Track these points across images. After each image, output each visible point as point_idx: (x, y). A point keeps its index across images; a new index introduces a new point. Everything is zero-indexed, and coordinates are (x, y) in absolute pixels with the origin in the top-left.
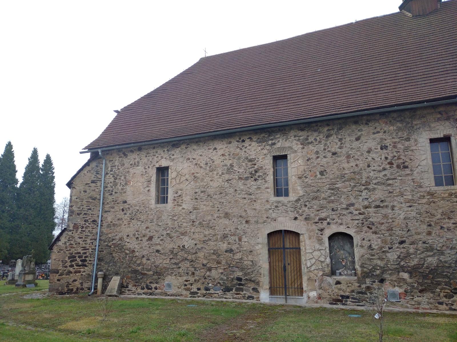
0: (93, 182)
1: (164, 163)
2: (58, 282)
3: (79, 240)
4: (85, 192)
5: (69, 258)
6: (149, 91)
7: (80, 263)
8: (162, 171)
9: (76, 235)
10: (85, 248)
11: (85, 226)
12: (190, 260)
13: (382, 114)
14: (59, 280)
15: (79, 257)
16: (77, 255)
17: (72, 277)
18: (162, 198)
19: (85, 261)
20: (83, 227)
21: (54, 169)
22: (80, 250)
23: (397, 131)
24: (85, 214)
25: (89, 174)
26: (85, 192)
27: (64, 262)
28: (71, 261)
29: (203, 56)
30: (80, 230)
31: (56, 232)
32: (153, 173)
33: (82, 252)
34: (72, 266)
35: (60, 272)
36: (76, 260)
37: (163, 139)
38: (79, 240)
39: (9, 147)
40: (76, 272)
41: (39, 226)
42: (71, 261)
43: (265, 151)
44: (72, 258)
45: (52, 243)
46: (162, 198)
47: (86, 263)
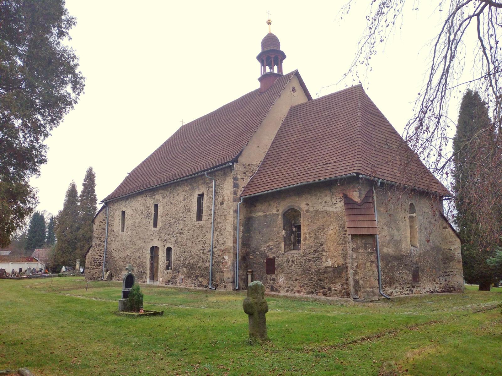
0: (104, 220)
1: (124, 209)
3: (98, 252)
4: (100, 225)
5: (93, 261)
8: (123, 213)
9: (96, 249)
10: (100, 256)
15: (98, 261)
17: (95, 271)
19: (100, 263)
22: (98, 257)
25: (102, 216)
26: (100, 225)
27: (91, 263)
28: (94, 263)
29: (181, 126)
31: (492, 122)
32: (121, 213)
34: (94, 265)
37: (177, 179)
38: (98, 252)
40: (96, 269)
41: (68, 248)
42: (94, 263)
43: (152, 202)
44: (95, 261)
45: (493, 125)
46: (123, 230)
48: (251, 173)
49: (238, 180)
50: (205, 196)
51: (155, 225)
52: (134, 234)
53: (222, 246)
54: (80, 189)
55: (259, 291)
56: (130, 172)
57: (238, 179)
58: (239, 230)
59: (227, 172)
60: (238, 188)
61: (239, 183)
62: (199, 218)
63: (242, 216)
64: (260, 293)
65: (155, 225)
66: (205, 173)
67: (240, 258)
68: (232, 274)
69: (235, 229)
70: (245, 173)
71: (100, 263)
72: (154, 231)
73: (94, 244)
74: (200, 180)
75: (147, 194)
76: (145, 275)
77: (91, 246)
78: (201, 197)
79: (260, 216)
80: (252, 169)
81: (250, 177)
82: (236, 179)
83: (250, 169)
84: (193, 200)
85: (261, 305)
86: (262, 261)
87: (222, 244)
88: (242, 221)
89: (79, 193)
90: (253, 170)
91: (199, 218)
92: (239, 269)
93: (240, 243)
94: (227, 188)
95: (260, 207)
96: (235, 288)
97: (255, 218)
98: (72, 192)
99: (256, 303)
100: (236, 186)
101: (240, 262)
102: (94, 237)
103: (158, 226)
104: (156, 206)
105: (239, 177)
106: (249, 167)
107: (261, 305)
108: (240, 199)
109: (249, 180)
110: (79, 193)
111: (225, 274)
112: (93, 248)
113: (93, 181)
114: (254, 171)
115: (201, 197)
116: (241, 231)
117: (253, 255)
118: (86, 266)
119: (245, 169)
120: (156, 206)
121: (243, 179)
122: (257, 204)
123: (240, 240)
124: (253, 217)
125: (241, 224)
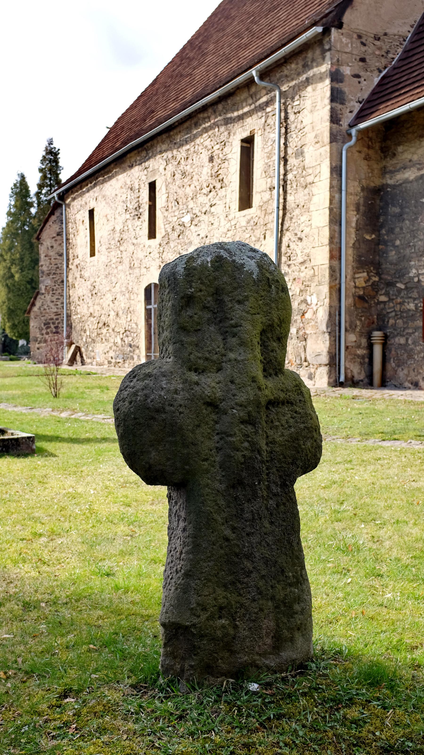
1: (92, 205)
2: (38, 351)
4: (52, 247)
5: (45, 324)
6: (213, 10)
7: (54, 330)
8: (91, 213)
11: (55, 288)
12: (308, 186)
13: (294, 55)
14: (38, 349)
15: (53, 323)
16: (51, 322)
18: (93, 254)
20: (53, 290)
21: (3, 229)
23: (381, 253)
24: (54, 274)
27: (41, 329)
30: (51, 292)
33: (55, 317)
34: (47, 333)
35: (39, 339)
36: (50, 327)
38: (51, 305)
39: (23, 177)
44: (47, 324)
46: (93, 254)
47: (59, 330)
48: (384, 61)
49: (341, 81)
50: (258, 140)
51: (152, 234)
52: (114, 260)
53: (303, 268)
54: (33, 182)
55: (238, 312)
56: (111, 125)
57: (343, 75)
58: (347, 222)
59: (313, 60)
60: (342, 103)
61: (346, 90)
62: (246, 202)
63: (356, 184)
64: (251, 330)
65: (152, 234)
66: (254, 73)
67: (351, 300)
68: (328, 343)
69: (335, 219)
70: (363, 60)
71: (56, 327)
72: (150, 246)
73: (42, 287)
74: (245, 100)
75: (133, 160)
76: (137, 351)
77: (38, 293)
78: (248, 144)
79: (406, 181)
80: (385, 47)
81: (380, 72)
82: (336, 77)
83: (380, 49)
84: (229, 156)
85: (250, 421)
86: (412, 306)
87: (302, 263)
88: (353, 199)
89: (33, 189)
90: (388, 52)
91: (246, 202)
92: (346, 330)
93: (351, 258)
94: (314, 107)
95: (407, 156)
96: (336, 381)
97: (394, 187)
98: (21, 189)
99: (212, 404)
100: (336, 97)
101: (348, 310)
102: (43, 272)
103: (158, 235)
104: (152, 186)
105: (347, 71)
106: (377, 43)
107: (250, 421)
108: (350, 135)
109: (376, 80)
110: (33, 189)
111: (309, 342)
112: (42, 297)
113: (56, 161)
114: (391, 55)
115: (248, 144)
116: (354, 225)
117: (387, 294)
118: (32, 335)
119: (363, 49)
120: (152, 186)
121: (357, 76)
122: (400, 149)
123: (350, 251)
124: (388, 185)
125: (352, 208)
